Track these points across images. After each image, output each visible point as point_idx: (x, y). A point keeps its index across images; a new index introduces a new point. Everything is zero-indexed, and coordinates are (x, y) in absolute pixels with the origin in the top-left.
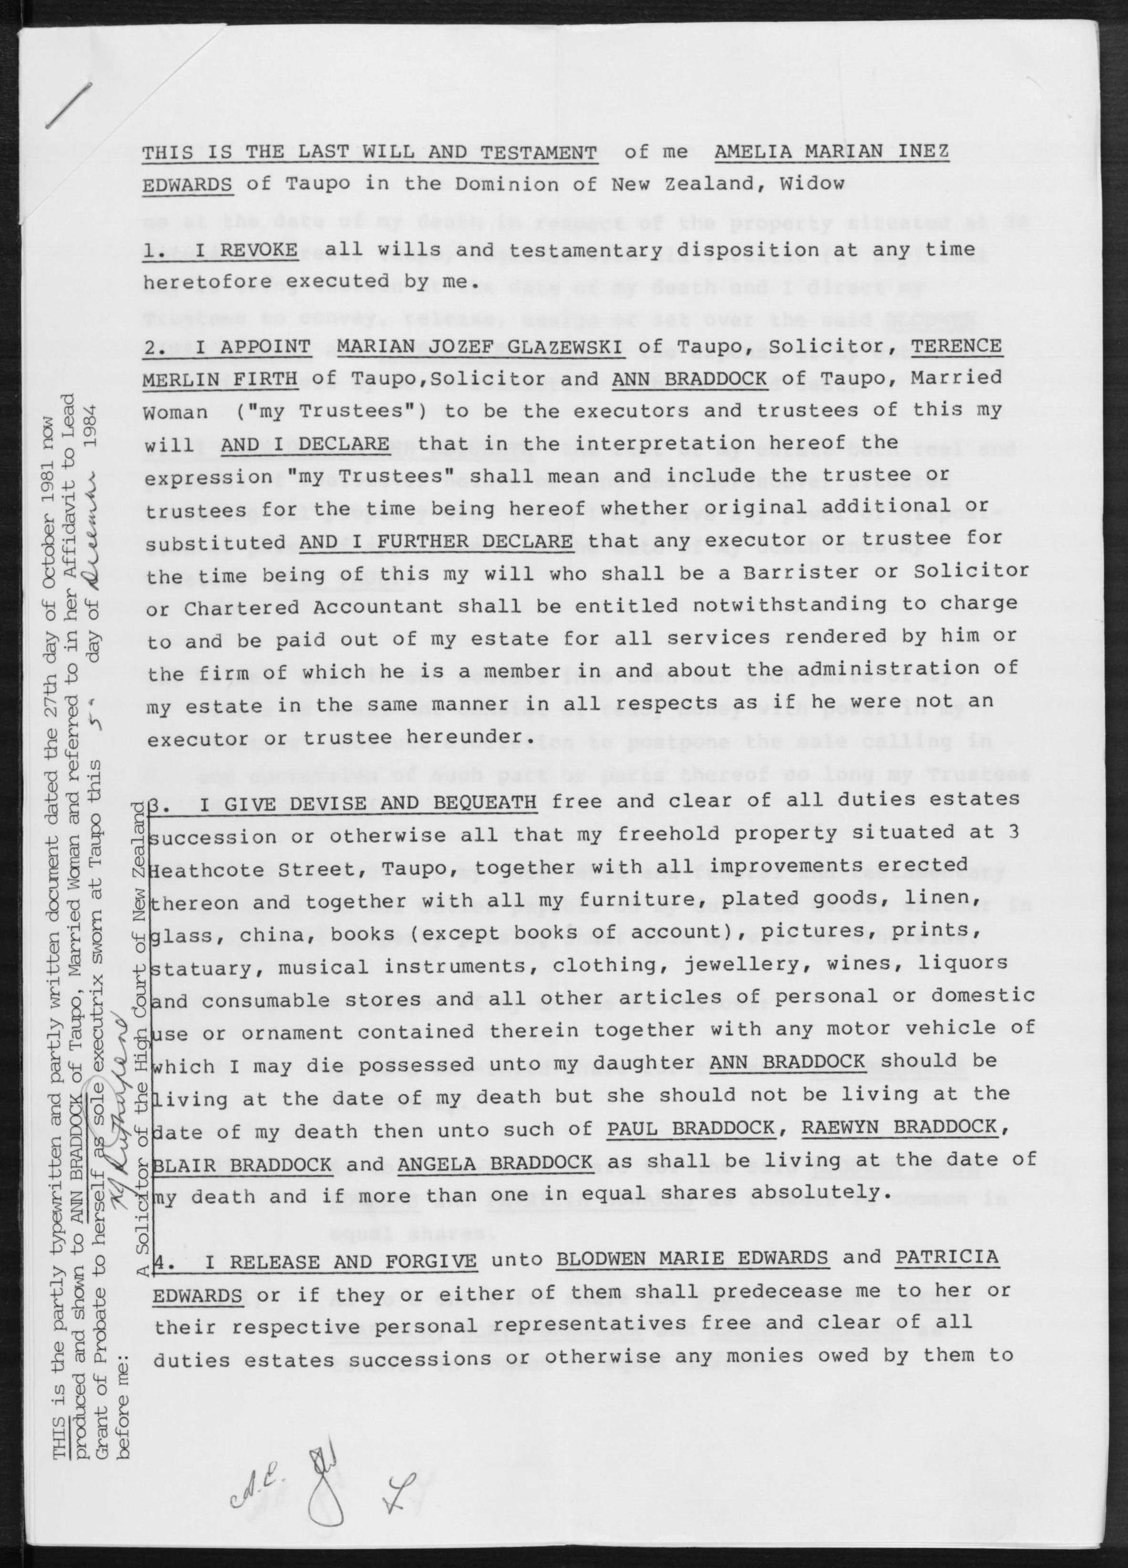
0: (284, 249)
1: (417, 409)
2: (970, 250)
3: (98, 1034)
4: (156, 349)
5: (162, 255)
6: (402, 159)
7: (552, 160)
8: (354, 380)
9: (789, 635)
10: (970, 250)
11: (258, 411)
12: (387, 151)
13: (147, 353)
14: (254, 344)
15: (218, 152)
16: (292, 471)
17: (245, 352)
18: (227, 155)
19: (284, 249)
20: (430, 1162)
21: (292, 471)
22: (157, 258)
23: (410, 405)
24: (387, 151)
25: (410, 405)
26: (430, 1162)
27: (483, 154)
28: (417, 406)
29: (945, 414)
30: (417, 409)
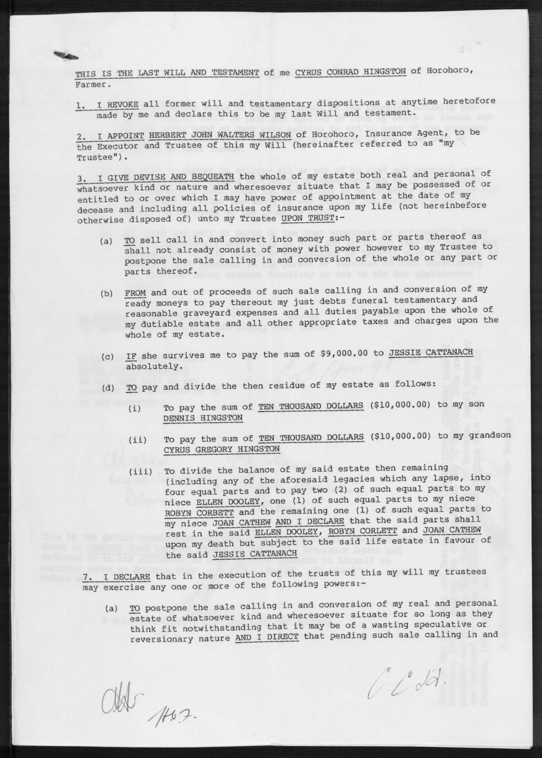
0: (133, 104)
1: (118, 156)
2: (480, 404)
4: (82, 137)
5: (83, 108)
6: (180, 76)
7: (241, 75)
8: (167, 146)
9: (270, 385)
10: (480, 404)
11: (443, 143)
12: (174, 73)
13: (78, 139)
14: (121, 135)
15: (106, 74)
16: (441, 141)
17: (117, 138)
19: (133, 104)
20: (256, 448)
21: (441, 141)
22: (82, 109)
23: (115, 155)
24: (174, 73)
25: (115, 155)
26: (256, 448)
27: (213, 73)
28: (118, 155)
29: (236, 147)
30: (118, 156)
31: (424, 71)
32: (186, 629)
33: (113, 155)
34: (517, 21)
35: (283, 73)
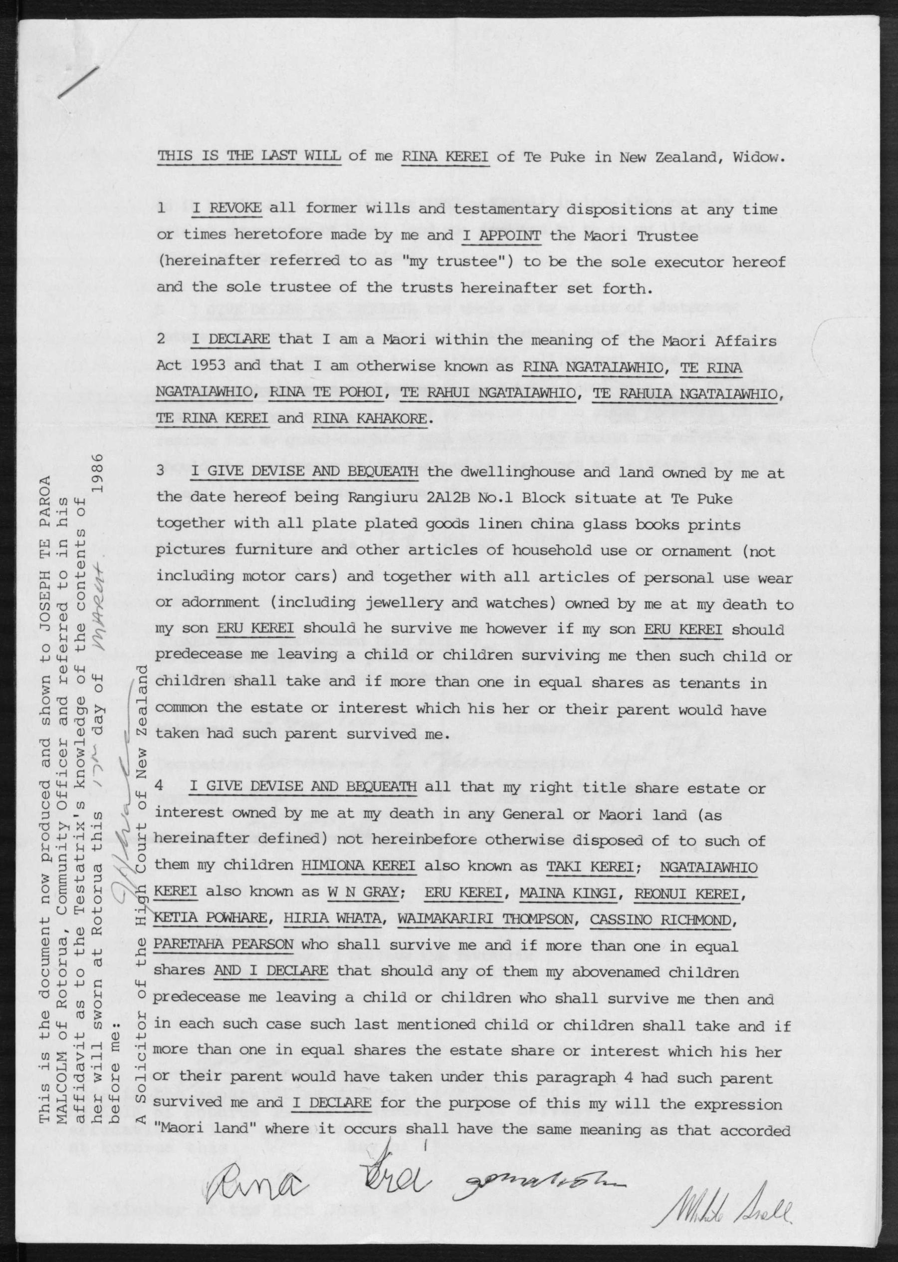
3: (685, 263)
18: (214, 157)
23: (502, 257)
25: (502, 257)
31: (370, 156)
32: (64, 721)
33: (497, 259)
34: (861, 34)
35: (379, 157)
